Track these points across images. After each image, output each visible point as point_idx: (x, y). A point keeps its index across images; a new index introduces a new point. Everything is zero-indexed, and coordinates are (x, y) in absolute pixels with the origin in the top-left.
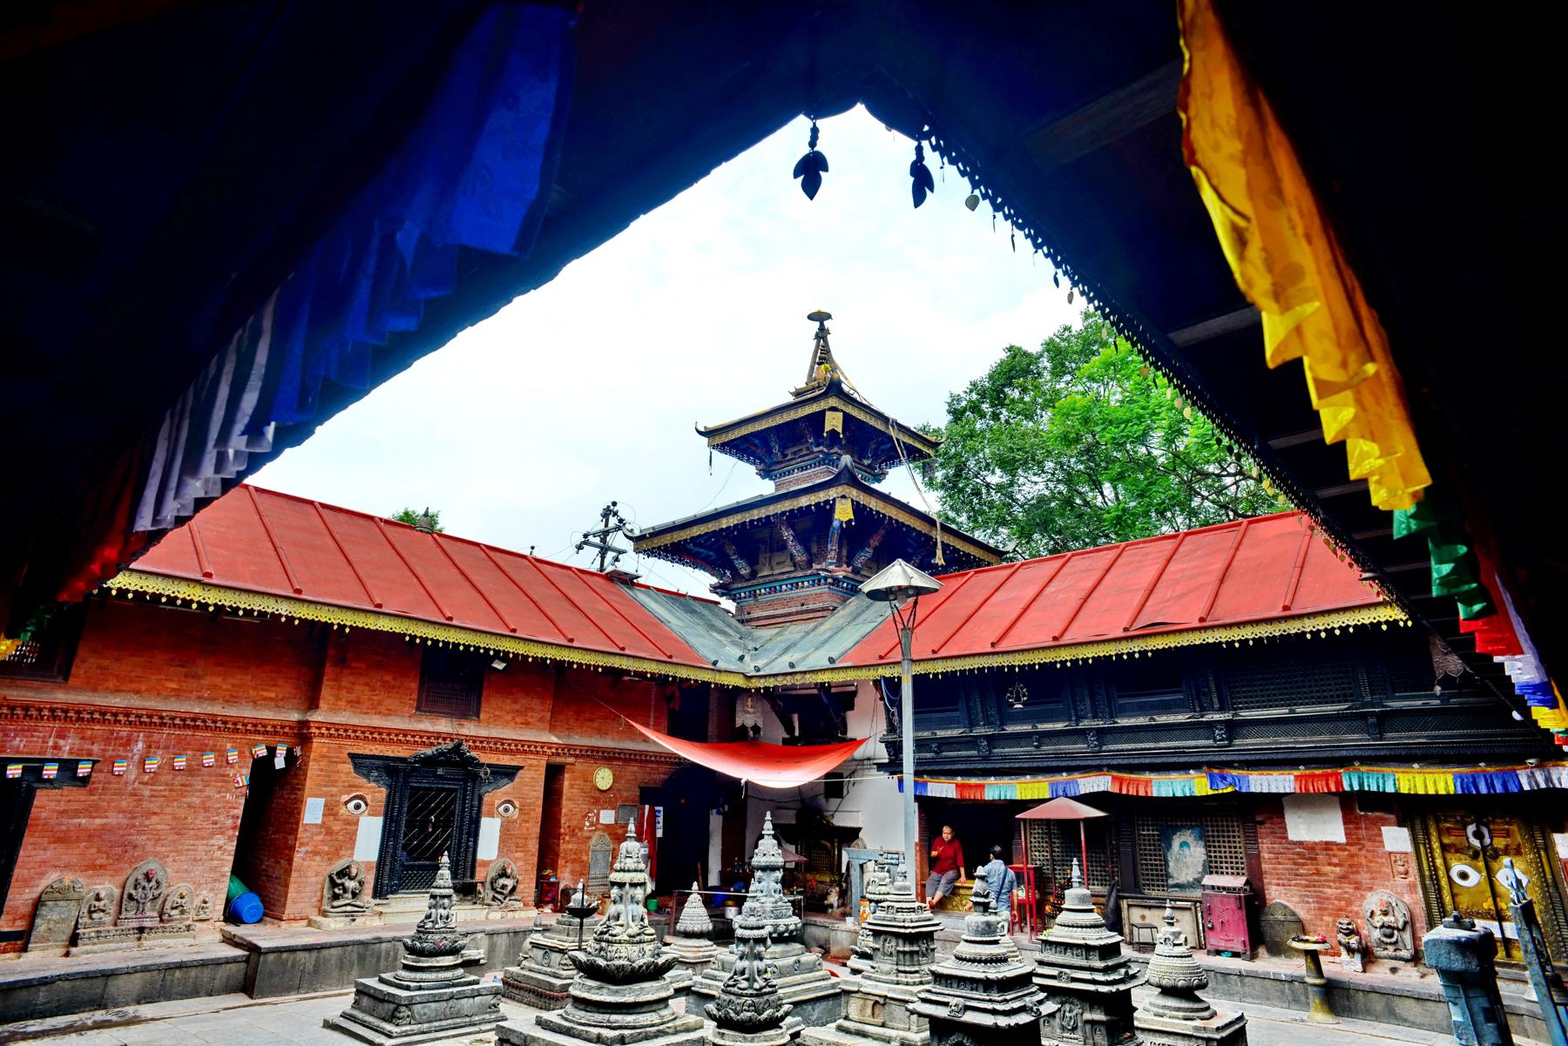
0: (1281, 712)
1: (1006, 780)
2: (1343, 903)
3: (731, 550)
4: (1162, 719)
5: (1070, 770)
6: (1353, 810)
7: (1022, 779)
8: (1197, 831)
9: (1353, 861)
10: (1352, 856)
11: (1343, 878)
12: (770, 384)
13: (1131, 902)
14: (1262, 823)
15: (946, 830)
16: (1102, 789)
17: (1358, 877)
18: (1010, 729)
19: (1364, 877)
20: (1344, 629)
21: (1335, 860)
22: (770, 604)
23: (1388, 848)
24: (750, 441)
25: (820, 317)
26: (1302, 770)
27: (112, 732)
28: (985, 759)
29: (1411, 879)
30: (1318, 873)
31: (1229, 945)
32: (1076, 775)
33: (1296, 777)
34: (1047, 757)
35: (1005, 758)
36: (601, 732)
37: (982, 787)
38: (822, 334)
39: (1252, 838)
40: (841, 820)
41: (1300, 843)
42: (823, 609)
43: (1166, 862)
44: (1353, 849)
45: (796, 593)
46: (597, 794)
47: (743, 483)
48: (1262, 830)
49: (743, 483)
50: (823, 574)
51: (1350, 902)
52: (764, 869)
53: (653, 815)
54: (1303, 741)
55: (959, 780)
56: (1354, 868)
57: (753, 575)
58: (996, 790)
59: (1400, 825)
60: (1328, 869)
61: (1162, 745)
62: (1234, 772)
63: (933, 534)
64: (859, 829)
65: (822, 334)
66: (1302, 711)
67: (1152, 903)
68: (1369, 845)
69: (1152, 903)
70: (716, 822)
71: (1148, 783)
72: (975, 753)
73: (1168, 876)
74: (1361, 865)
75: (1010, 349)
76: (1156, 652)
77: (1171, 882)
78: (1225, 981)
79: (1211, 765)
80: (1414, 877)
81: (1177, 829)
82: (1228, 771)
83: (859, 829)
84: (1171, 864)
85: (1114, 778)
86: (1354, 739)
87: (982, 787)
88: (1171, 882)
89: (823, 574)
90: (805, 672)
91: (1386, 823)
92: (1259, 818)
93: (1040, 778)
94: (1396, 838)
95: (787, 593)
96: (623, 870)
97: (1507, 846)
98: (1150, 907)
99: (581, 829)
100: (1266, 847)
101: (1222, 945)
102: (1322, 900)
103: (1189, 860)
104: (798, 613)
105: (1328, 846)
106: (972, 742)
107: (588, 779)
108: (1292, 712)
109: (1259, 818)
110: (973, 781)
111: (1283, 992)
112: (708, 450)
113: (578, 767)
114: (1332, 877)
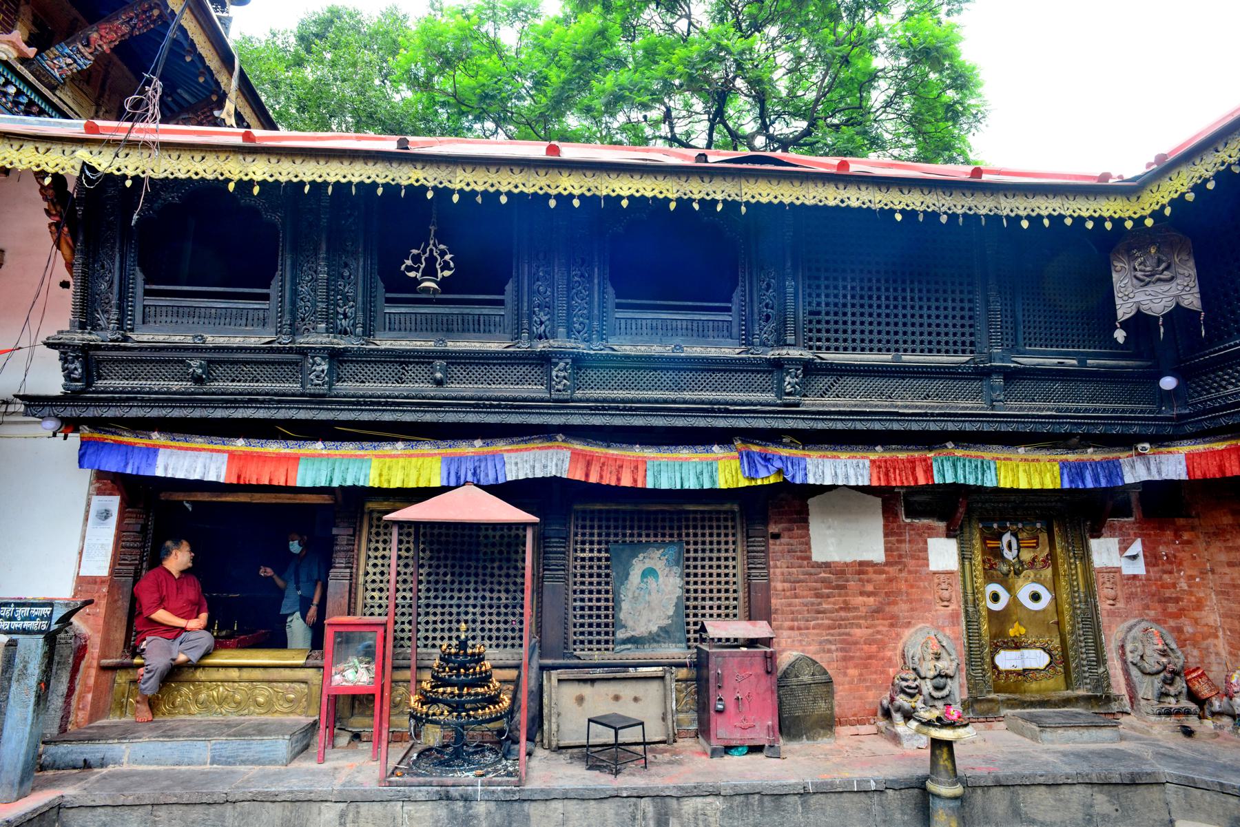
0: (885, 358)
1: (349, 448)
2: (874, 648)
6: (896, 516)
7: (387, 448)
8: (672, 552)
9: (891, 585)
10: (890, 580)
13: (565, 674)
14: (776, 536)
16: (552, 471)
17: (895, 609)
18: (385, 343)
19: (901, 609)
20: (1057, 220)
21: (869, 588)
23: (933, 567)
26: (879, 453)
27: (1096, 688)
29: (953, 607)
30: (846, 607)
31: (748, 735)
32: (500, 446)
33: (873, 462)
34: (459, 404)
41: (827, 565)
43: (617, 601)
44: (892, 570)
48: (775, 547)
51: (882, 645)
54: (909, 402)
55: (240, 444)
58: (317, 467)
59: (948, 536)
61: (687, 395)
62: (785, 452)
67: (598, 673)
68: (911, 563)
69: (598, 673)
71: (636, 466)
72: (295, 387)
73: (617, 625)
74: (899, 592)
77: (621, 635)
78: (777, 808)
79: (750, 435)
80: (956, 606)
81: (637, 548)
82: (772, 449)
84: (625, 606)
85: (575, 454)
86: (967, 403)
88: (621, 635)
91: (932, 532)
92: (773, 529)
93: (426, 448)
94: (943, 553)
97: (1034, 560)
100: (780, 570)
101: (736, 737)
102: (848, 645)
105: (862, 567)
109: (773, 529)
110: (274, 448)
111: (868, 812)
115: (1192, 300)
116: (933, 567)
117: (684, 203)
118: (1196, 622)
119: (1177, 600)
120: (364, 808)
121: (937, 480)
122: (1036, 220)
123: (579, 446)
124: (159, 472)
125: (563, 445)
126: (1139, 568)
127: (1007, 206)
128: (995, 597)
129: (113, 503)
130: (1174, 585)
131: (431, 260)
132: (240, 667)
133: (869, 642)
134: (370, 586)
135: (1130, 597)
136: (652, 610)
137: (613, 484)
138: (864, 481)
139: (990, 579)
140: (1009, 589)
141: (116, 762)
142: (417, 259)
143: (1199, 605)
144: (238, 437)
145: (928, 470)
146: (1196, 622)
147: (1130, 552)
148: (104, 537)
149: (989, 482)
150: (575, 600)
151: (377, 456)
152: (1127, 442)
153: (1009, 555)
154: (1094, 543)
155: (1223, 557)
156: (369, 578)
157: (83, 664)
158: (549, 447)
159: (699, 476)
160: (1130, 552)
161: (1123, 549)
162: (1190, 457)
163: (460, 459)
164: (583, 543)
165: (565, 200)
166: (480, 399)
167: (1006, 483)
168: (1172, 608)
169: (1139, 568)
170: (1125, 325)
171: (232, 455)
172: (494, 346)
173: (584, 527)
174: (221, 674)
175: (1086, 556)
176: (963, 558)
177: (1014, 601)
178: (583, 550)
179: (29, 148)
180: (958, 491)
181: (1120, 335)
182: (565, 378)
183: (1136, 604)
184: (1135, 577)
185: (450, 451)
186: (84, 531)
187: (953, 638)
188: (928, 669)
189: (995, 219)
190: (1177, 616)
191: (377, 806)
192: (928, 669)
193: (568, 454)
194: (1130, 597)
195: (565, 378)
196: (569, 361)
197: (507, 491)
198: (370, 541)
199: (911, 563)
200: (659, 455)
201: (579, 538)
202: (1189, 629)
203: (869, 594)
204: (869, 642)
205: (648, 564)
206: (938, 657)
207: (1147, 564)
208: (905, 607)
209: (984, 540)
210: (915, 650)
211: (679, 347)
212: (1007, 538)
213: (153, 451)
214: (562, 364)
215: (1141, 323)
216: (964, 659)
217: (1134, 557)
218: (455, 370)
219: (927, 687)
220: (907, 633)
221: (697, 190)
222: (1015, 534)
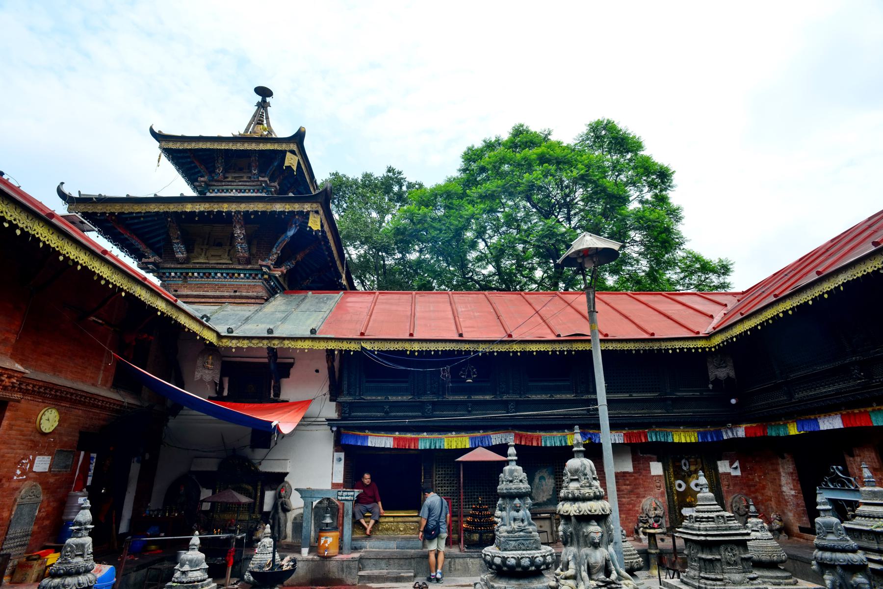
3: (175, 234)
4: (558, 397)
5: (486, 428)
11: (631, 492)
12: (225, 118)
15: (367, 476)
19: (641, 490)
20: (682, 349)
21: (628, 482)
22: (200, 287)
23: (653, 473)
24: (188, 155)
25: (264, 92)
36: (55, 369)
37: (417, 440)
38: (263, 106)
40: (268, 467)
42: (257, 298)
45: (228, 281)
46: (37, 438)
47: (171, 183)
49: (171, 183)
50: (265, 269)
51: (634, 506)
52: (511, 496)
53: (87, 459)
56: (636, 486)
57: (187, 260)
58: (425, 442)
62: (591, 432)
64: (286, 474)
65: (263, 106)
66: (635, 396)
68: (644, 472)
70: (135, 469)
75: (612, 139)
76: (577, 352)
83: (286, 474)
86: (658, 412)
87: (417, 440)
89: (265, 269)
90: (284, 339)
93: (463, 434)
94: (656, 468)
95: (219, 278)
96: (575, 499)
99: (10, 479)
103: (545, 487)
104: (230, 297)
107: (31, 419)
108: (631, 396)
112: (160, 151)
113: (23, 405)
114: (626, 492)
115: (732, 374)
116: (653, 473)
117: (554, 352)
118: (763, 494)
119: (755, 486)
120: (457, 560)
121: (649, 440)
122: (674, 350)
124: (369, 445)
126: (738, 473)
127: (664, 345)
128: (680, 486)
129: (342, 455)
130: (753, 480)
131: (469, 372)
132: (394, 517)
133: (629, 504)
135: (735, 485)
136: (544, 492)
138: (621, 441)
139: (677, 478)
140: (686, 482)
141: (365, 548)
142: (464, 371)
143: (764, 488)
145: (646, 437)
146: (763, 494)
147: (734, 466)
148: (340, 468)
149: (670, 440)
152: (723, 424)
153: (685, 468)
154: (719, 463)
155: (770, 467)
159: (561, 441)
160: (734, 466)
161: (731, 465)
162: (746, 428)
163: (475, 438)
165: (515, 353)
167: (676, 440)
168: (753, 489)
169: (738, 473)
170: (712, 383)
171: (395, 438)
172: (488, 398)
174: (387, 520)
175: (716, 468)
176: (664, 470)
177: (688, 488)
179: (345, 342)
180: (657, 443)
181: (711, 386)
183: (737, 487)
184: (736, 476)
187: (662, 501)
188: (652, 514)
189: (660, 350)
190: (754, 492)
191: (461, 560)
192: (652, 514)
194: (735, 485)
199: (644, 472)
202: (760, 498)
203: (628, 485)
204: (629, 504)
205: (541, 474)
206: (655, 509)
207: (741, 471)
208: (642, 490)
209: (674, 463)
210: (647, 507)
211: (552, 396)
212: (683, 461)
213: (366, 437)
215: (717, 381)
216: (667, 511)
217: (736, 468)
219: (651, 521)
220: (644, 500)
221: (558, 347)
222: (687, 459)
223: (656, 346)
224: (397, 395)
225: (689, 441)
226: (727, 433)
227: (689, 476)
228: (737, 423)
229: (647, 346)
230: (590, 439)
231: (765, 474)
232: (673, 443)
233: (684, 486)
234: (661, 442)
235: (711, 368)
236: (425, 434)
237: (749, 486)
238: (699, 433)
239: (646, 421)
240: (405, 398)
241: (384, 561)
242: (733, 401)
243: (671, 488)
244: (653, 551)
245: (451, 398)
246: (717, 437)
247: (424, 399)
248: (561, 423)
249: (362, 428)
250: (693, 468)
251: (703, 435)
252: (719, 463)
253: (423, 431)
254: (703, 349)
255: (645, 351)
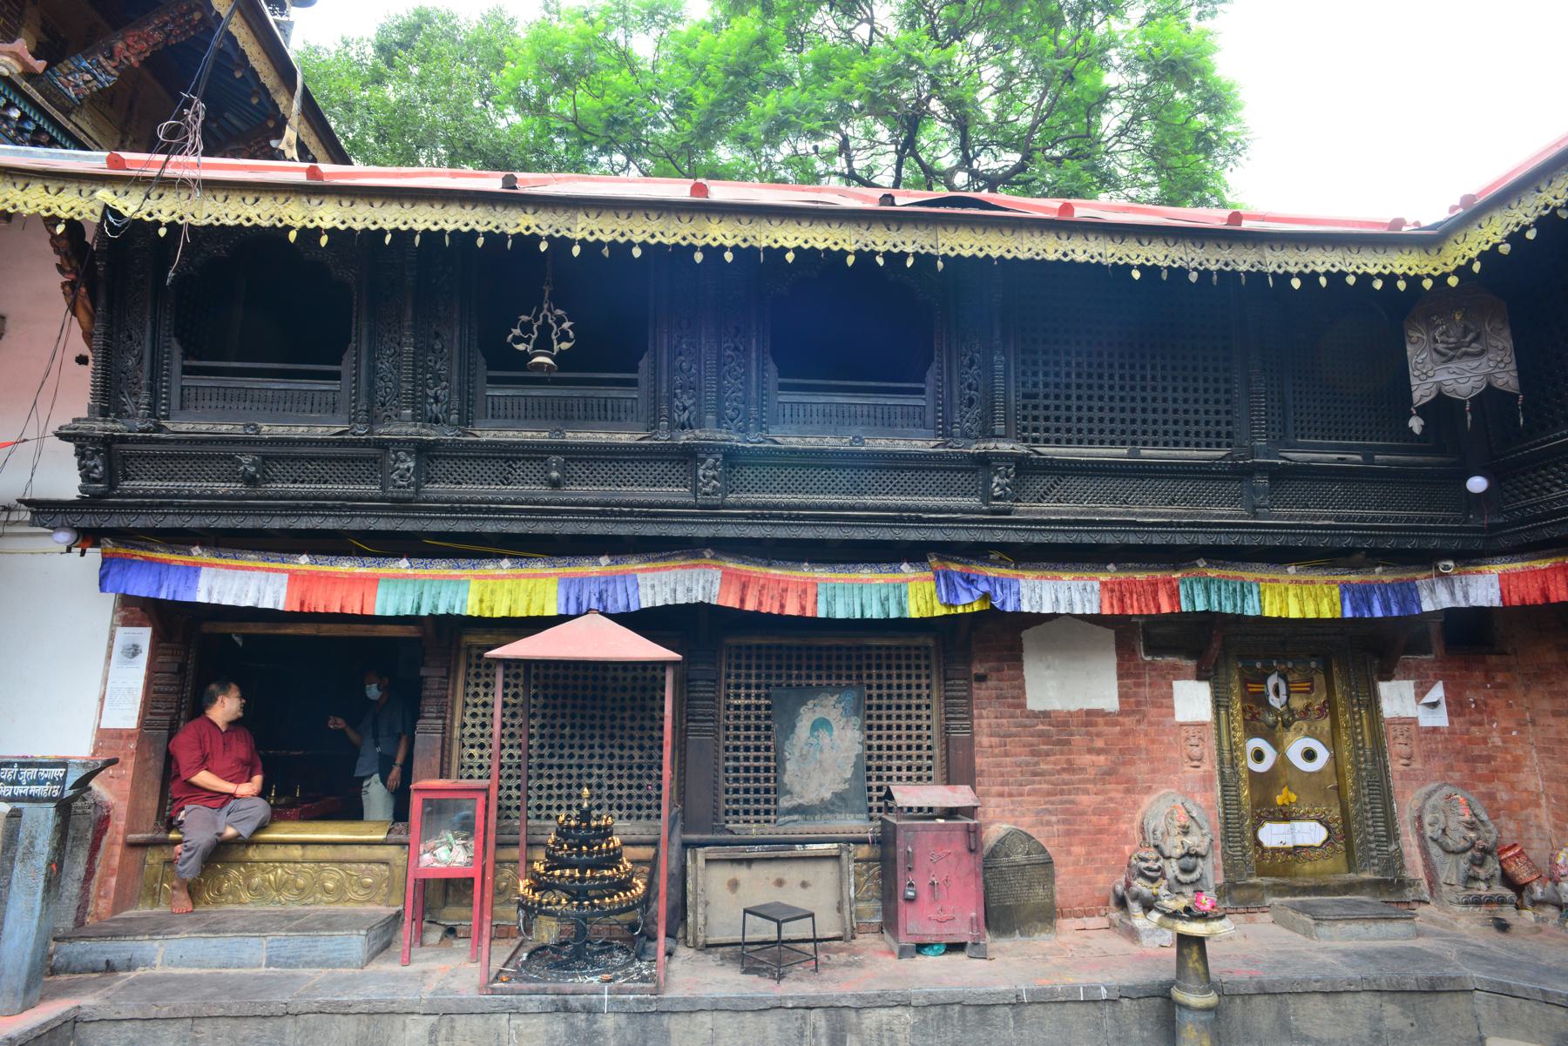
0: (1118, 453)
1: (441, 568)
2: (1105, 819)
7: (490, 568)
8: (850, 697)
11: (1109, 773)
13: (714, 853)
14: (981, 678)
16: (698, 596)
17: (1131, 771)
19: (1140, 770)
20: (1337, 278)
21: (1099, 743)
26: (1110, 574)
28: (401, 506)
29: (1206, 767)
30: (1070, 768)
32: (633, 565)
33: (1104, 584)
34: (581, 510)
35: (455, 508)
39: (958, 710)
41: (1045, 715)
44: (1128, 721)
48: (981, 692)
51: (1116, 816)
54: (1150, 510)
56: (1128, 755)
58: (397, 591)
59: (1199, 678)
60: (1087, 759)
61: (869, 500)
62: (992, 572)
63: (281, 100)
67: (757, 851)
68: (1153, 712)
69: (757, 851)
72: (374, 489)
74: (1138, 749)
77: (785, 803)
78: (983, 1022)
79: (948, 550)
80: (1209, 766)
81: (806, 693)
82: (977, 569)
85: (727, 574)
86: (1223, 512)
88: (785, 803)
92: (978, 669)
93: (539, 567)
94: (1192, 700)
97: (1307, 708)
98: (749, 861)
100: (986, 722)
101: (931, 932)
106: (367, 456)
109: (978, 669)
110: (346, 567)
111: (1098, 1026)
115: (1507, 379)
117: (865, 257)
118: (1512, 786)
119: (1488, 759)
120: (460, 1022)
121: (1185, 607)
122: (1310, 279)
123: (732, 565)
124: (202, 597)
125: (713, 562)
126: (1440, 719)
127: (1274, 261)
128: (1259, 756)
129: (143, 636)
130: (1485, 741)
131: (545, 330)
132: (304, 843)
133: (1099, 812)
134: (467, 742)
135: (1429, 756)
137: (775, 612)
138: (1092, 609)
139: (1251, 732)
141: (148, 963)
142: (527, 328)
143: (1517, 765)
144: (301, 553)
145: (1174, 595)
146: (1512, 786)
148: (131, 679)
149: (1251, 610)
150: (727, 759)
151: (477, 577)
152: (1425, 559)
153: (1276, 702)
154: (1384, 687)
156: (467, 731)
157: (105, 840)
158: (695, 566)
159: (884, 602)
161: (1420, 693)
162: (1504, 579)
163: (582, 581)
164: (738, 687)
166: (607, 504)
167: (1272, 610)
168: (1482, 769)
169: (1440, 719)
170: (1423, 411)
171: (293, 576)
172: (624, 438)
173: (738, 667)
174: (279, 853)
175: (1373, 703)
178: (737, 696)
180: (1209, 620)
181: (1416, 424)
182: (714, 477)
183: (1436, 764)
185: (569, 570)
186: (106, 672)
187: (1205, 805)
190: (1488, 779)
193: (719, 574)
194: (1429, 756)
195: (714, 477)
196: (720, 456)
197: (640, 621)
198: (467, 684)
200: (833, 576)
201: (732, 681)
202: (1503, 796)
203: (1099, 752)
204: (1099, 812)
205: (820, 713)
206: (1185, 831)
207: (1450, 714)
208: (1144, 767)
209: (1245, 683)
210: (1157, 823)
212: (1273, 680)
213: (195, 569)
214: (710, 461)
215: (1442, 407)
217: (1434, 705)
218: (576, 468)
219: (1172, 869)
220: (1147, 800)
221: (881, 240)
222: (1283, 676)
223: (1244, 260)
224: (298, 422)
225: (1311, 615)
226: (1432, 591)
227: (1287, 725)
228: (1470, 557)
229: (1213, 259)
230: (986, 597)
231: (1521, 725)
232: (1261, 620)
233: (1270, 755)
234: (1221, 615)
235: (1419, 357)
236: (404, 563)
237: (1472, 760)
238: (1345, 588)
239: (1179, 540)
240: (320, 432)
241: (177, 1027)
242: (1477, 484)
243: (1233, 764)
244: (1195, 1000)
245: (487, 436)
246: (1403, 605)
247: (384, 432)
248: (887, 535)
249: (179, 539)
250: (1298, 703)
251: (1361, 596)
252: (1384, 687)
253: (397, 555)
254: (1414, 281)
255: (1205, 274)
